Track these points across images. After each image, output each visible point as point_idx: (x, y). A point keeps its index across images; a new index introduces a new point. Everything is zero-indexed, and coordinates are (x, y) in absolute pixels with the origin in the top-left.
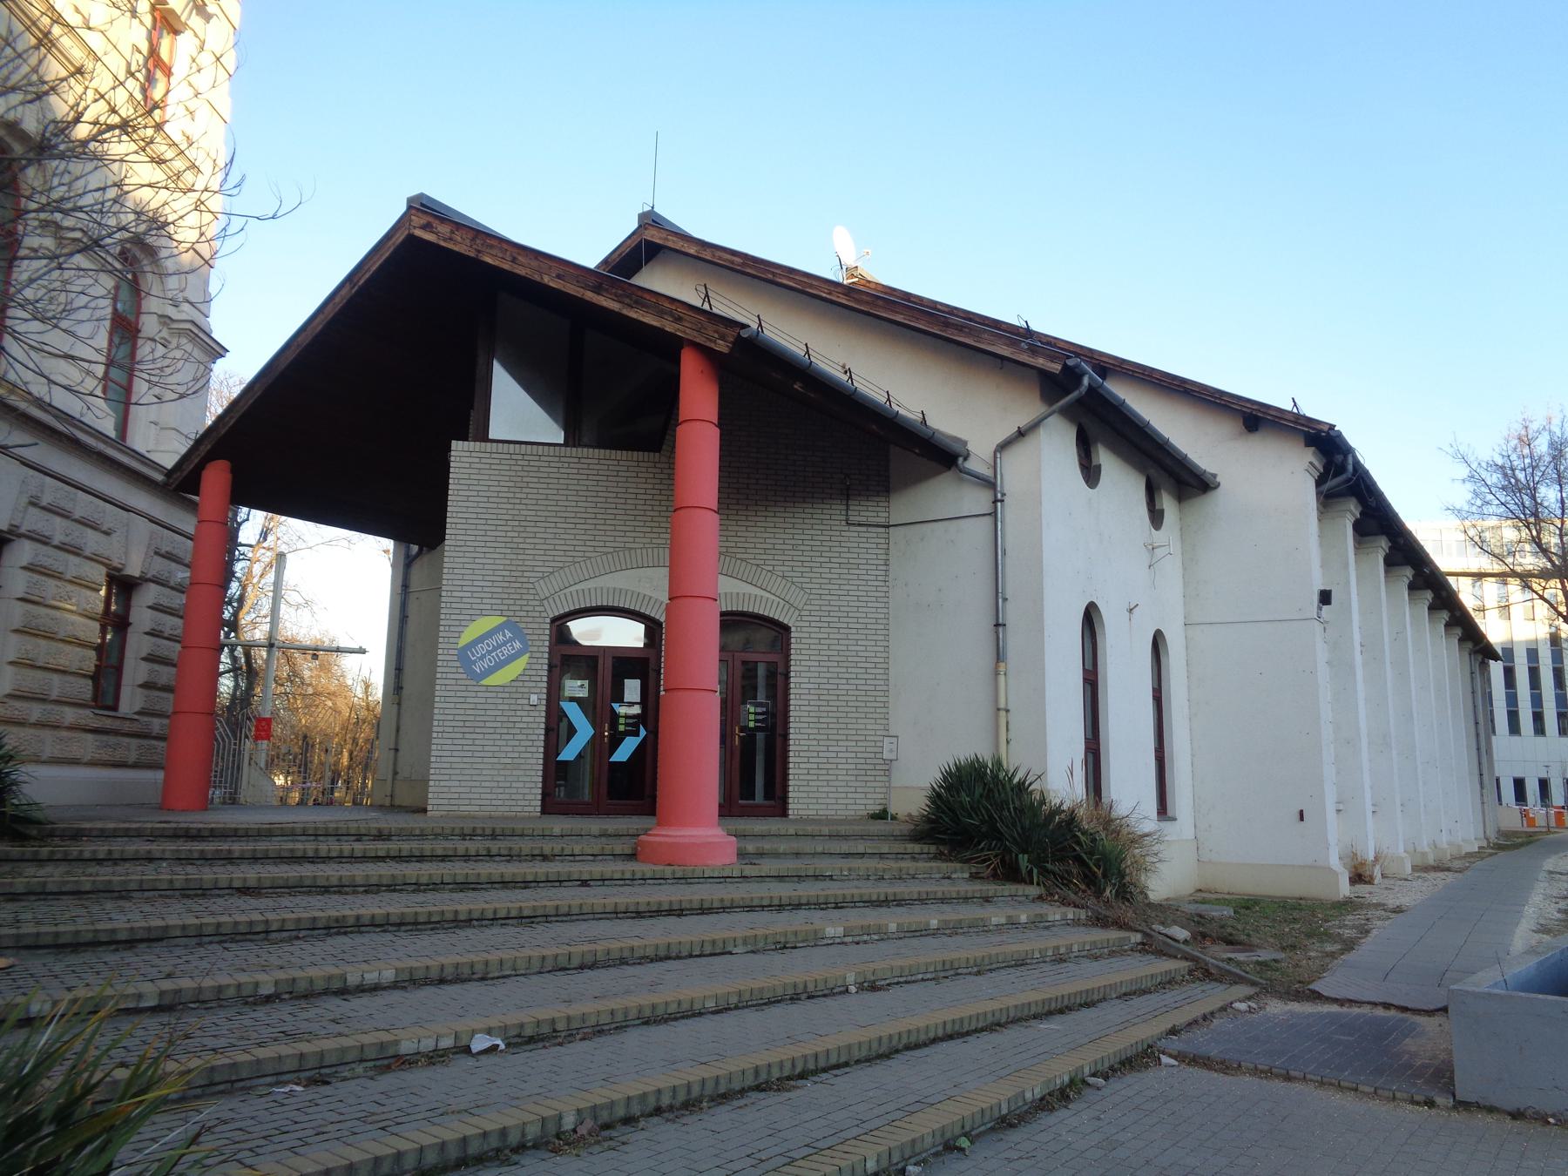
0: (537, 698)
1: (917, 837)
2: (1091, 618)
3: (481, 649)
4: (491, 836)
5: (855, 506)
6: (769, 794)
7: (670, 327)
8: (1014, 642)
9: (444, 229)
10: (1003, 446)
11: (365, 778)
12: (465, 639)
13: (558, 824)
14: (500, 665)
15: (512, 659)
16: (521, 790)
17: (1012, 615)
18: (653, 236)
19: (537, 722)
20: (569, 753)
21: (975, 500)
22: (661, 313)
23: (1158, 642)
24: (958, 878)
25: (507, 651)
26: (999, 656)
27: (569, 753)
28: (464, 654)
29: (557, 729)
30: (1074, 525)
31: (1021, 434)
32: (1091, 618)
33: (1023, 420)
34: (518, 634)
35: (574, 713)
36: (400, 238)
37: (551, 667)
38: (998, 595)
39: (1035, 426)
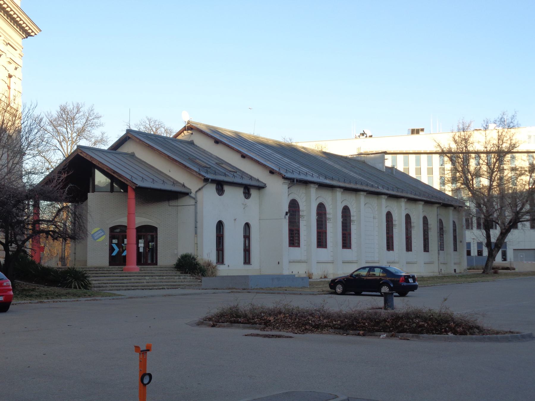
0: (107, 243)
1: (175, 268)
2: (220, 225)
3: (96, 234)
4: (98, 270)
5: (170, 202)
6: (152, 261)
7: (126, 182)
8: (199, 230)
9: (85, 154)
10: (197, 192)
11: (138, 243)
12: (92, 233)
13: (111, 267)
14: (100, 237)
15: (102, 236)
16: (104, 261)
17: (199, 225)
18: (129, 135)
19: (107, 248)
20: (114, 254)
21: (192, 202)
22: (124, 180)
23: (247, 226)
24: (179, 273)
25: (101, 234)
26: (196, 233)
27: (114, 254)
28: (92, 235)
29: (112, 250)
30: (211, 206)
31: (200, 189)
32: (220, 225)
33: (200, 186)
34: (103, 231)
35: (115, 246)
36: (76, 154)
37: (110, 237)
38: (196, 222)
39: (202, 188)
